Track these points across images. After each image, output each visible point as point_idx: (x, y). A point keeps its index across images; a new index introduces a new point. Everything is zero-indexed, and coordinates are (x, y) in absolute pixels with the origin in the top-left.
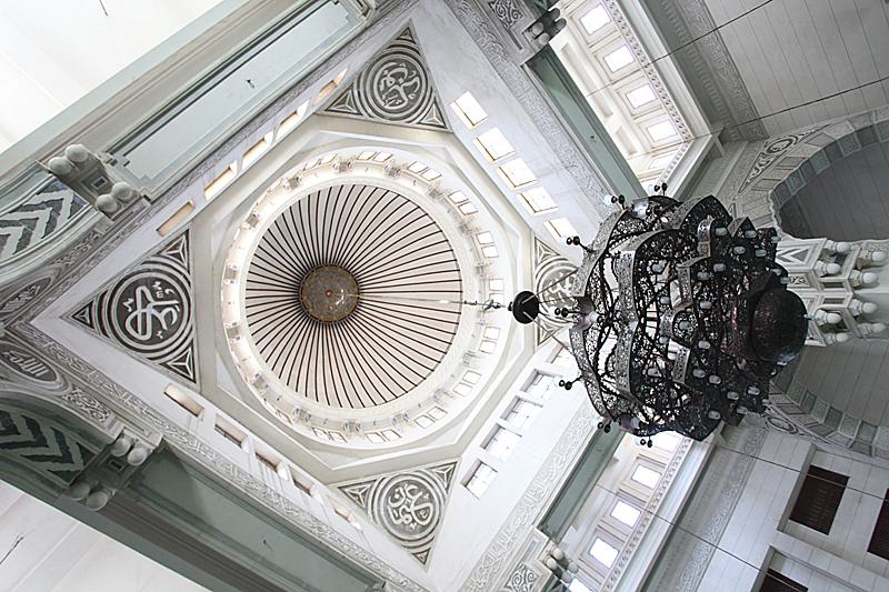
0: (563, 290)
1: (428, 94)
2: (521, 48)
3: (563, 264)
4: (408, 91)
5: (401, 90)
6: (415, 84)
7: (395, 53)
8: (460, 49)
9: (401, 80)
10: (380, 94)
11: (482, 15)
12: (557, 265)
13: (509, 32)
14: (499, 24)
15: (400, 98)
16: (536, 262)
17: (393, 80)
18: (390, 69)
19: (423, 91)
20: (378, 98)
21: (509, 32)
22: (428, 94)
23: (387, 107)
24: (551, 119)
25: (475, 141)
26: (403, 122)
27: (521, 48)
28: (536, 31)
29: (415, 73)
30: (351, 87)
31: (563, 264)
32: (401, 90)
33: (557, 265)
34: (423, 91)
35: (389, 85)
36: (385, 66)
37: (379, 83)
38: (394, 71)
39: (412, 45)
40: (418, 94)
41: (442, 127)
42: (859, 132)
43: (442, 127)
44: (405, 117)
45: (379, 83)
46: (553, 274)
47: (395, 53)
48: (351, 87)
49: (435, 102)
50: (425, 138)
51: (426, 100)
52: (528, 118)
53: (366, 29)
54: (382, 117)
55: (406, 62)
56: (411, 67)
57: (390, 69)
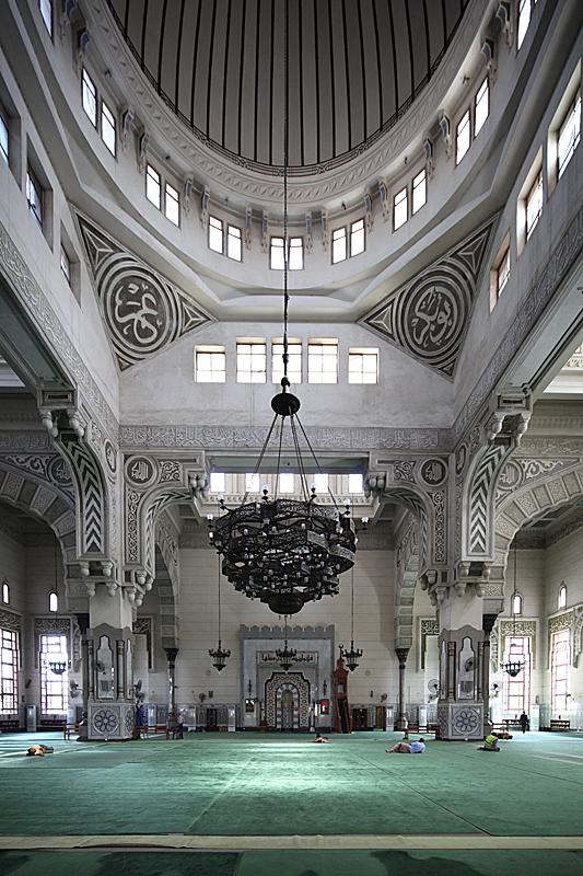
0: (141, 312)
1: (402, 338)
2: (379, 462)
3: (169, 333)
4: (422, 323)
5: (428, 319)
6: (418, 337)
7: (450, 348)
8: (407, 410)
9: (433, 328)
10: (445, 297)
11: (414, 451)
12: (171, 326)
13: (392, 462)
14: (401, 458)
15: (424, 311)
16: (185, 300)
17: (440, 322)
18: (449, 328)
19: (408, 336)
20: (445, 291)
21: (392, 462)
22: (402, 338)
23: (431, 290)
24: (322, 445)
25: (335, 341)
26: (408, 287)
27: (379, 462)
28: (381, 482)
29: (425, 346)
30: (475, 278)
31: (169, 333)
32: (428, 319)
33: (171, 326)
34: (408, 336)
35: (442, 314)
36: (453, 327)
37: (451, 307)
38: (444, 329)
39: (440, 366)
40: (411, 328)
41: (367, 318)
42: (173, 598)
43: (367, 318)
44: (409, 295)
45: (451, 307)
46: (163, 312)
47: (450, 348)
48: (475, 278)
49: (391, 336)
50: (375, 293)
51: (400, 330)
52: (331, 425)
53: (493, 388)
54: (430, 275)
55: (439, 348)
56: (432, 347)
57: (449, 328)
